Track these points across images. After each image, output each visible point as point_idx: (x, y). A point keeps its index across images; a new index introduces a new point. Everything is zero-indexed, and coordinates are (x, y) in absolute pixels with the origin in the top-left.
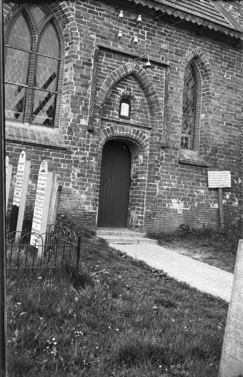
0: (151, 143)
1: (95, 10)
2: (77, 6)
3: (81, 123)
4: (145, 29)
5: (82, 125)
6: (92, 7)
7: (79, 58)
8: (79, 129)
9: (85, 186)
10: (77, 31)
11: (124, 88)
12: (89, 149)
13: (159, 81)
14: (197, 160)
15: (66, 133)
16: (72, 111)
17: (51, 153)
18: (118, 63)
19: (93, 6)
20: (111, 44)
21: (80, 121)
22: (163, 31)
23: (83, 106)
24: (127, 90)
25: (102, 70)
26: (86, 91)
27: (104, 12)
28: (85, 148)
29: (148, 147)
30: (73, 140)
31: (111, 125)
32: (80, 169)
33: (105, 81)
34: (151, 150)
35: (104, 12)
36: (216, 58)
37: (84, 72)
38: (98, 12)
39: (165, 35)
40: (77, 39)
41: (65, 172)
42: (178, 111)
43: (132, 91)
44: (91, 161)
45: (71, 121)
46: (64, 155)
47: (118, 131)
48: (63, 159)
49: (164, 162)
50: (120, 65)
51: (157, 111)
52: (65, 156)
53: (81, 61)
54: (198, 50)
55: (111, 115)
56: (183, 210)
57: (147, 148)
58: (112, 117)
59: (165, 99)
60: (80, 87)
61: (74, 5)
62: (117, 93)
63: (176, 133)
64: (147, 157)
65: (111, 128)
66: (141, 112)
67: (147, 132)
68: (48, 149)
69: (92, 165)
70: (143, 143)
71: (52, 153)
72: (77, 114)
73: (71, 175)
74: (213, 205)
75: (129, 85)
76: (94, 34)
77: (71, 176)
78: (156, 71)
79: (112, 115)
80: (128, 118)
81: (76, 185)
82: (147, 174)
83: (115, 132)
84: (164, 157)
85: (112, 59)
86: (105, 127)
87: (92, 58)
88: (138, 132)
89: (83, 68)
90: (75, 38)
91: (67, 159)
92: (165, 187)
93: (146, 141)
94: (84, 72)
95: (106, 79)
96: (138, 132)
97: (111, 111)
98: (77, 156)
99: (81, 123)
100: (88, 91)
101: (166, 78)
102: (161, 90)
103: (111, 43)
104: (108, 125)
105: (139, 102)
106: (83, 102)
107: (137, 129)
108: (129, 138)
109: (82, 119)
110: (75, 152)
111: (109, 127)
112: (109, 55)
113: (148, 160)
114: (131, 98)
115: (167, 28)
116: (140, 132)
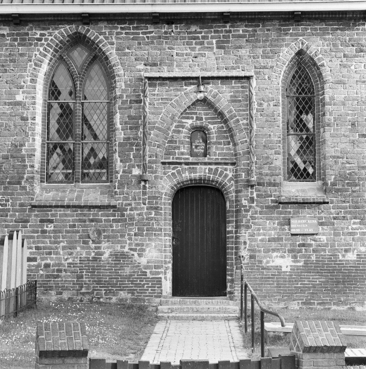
0: (236, 182)
1: (141, 35)
2: (118, 38)
3: (133, 173)
4: (212, 38)
5: (135, 176)
6: (136, 32)
7: (125, 96)
8: (132, 181)
11: (192, 118)
13: (240, 99)
14: (303, 195)
15: (116, 188)
16: (121, 161)
17: (100, 213)
19: (138, 31)
21: (131, 171)
22: (241, 31)
23: (134, 152)
24: (196, 120)
26: (137, 134)
27: (153, 34)
28: (141, 202)
29: (233, 188)
31: (178, 167)
32: (137, 227)
33: (161, 116)
35: (153, 34)
36: (334, 45)
37: (133, 112)
38: (145, 36)
39: (244, 36)
41: (119, 233)
43: (204, 120)
44: (150, 216)
45: (121, 173)
48: (114, 218)
52: (117, 215)
53: (127, 100)
54: (300, 42)
56: (291, 266)
57: (231, 189)
60: (128, 131)
61: (113, 37)
62: (183, 127)
64: (233, 200)
65: (179, 172)
66: (220, 143)
68: (96, 210)
69: (152, 220)
70: (226, 183)
71: (101, 214)
72: (128, 164)
73: (126, 235)
74: (344, 256)
75: (200, 113)
76: (141, 64)
77: (127, 237)
79: (178, 155)
81: (133, 247)
83: (183, 175)
86: (169, 172)
87: (141, 93)
88: (217, 169)
89: (131, 108)
91: (119, 218)
92: (260, 238)
94: (133, 112)
96: (217, 169)
97: (177, 151)
98: (132, 212)
99: (133, 173)
100: (139, 133)
102: (244, 111)
104: (173, 169)
105: (215, 131)
106: (134, 148)
107: (213, 167)
109: (135, 168)
110: (129, 207)
111: (174, 171)
114: (205, 129)
115: (246, 26)
116: (220, 170)
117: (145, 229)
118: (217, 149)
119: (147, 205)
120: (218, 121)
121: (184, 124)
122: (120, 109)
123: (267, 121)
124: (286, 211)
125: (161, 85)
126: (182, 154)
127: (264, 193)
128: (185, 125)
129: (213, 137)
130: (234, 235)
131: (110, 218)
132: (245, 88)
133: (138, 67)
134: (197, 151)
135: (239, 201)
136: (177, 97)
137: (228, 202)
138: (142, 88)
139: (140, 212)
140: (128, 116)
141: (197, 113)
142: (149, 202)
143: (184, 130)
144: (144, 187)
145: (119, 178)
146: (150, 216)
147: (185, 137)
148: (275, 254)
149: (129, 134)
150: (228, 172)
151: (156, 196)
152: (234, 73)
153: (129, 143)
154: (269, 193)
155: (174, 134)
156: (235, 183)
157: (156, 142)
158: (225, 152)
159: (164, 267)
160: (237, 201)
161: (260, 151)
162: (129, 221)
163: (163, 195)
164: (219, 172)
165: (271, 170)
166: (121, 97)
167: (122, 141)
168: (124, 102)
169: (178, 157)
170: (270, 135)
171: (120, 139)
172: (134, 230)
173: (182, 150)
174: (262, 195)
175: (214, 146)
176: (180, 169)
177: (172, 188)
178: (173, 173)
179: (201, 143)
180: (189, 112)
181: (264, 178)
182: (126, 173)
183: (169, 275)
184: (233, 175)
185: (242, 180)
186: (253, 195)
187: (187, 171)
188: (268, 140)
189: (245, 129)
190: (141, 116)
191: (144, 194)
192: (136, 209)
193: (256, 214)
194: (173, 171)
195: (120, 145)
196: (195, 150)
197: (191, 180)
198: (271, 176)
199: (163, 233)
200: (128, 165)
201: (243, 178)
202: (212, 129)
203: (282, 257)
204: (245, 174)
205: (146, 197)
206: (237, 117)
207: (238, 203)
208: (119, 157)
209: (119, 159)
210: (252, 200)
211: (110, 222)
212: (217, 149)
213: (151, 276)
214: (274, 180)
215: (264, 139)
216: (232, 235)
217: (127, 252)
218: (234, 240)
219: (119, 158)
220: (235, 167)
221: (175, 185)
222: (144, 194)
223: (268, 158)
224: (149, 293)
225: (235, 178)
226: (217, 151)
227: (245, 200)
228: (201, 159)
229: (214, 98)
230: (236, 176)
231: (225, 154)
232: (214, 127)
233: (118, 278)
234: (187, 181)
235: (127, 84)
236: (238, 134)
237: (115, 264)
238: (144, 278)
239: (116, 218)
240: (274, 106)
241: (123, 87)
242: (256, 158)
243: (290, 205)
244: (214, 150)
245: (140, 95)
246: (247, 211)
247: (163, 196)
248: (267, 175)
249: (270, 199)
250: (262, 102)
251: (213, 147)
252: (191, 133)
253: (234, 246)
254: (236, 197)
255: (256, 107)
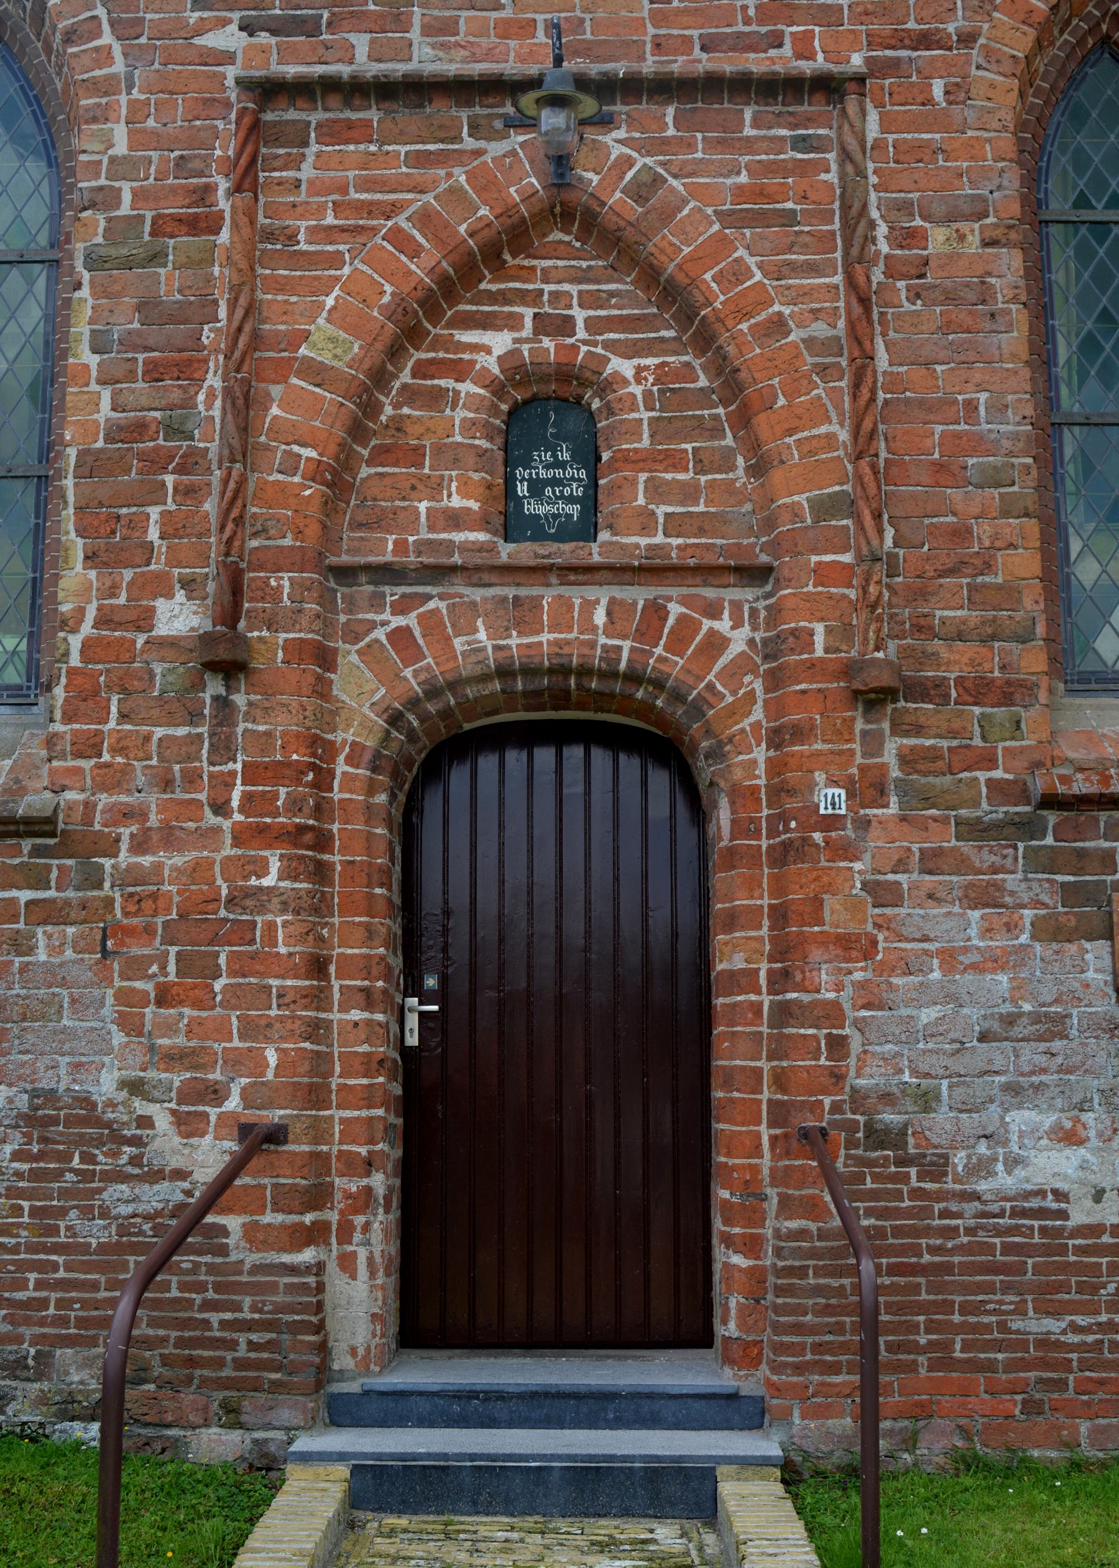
0: (774, 680)
3: (162, 629)
5: (171, 643)
7: (127, 197)
8: (152, 675)
9: (216, 1075)
10: (107, 38)
11: (513, 323)
12: (235, 803)
13: (789, 205)
15: (58, 715)
16: (90, 558)
18: (420, 160)
20: (362, 52)
23: (171, 506)
24: (537, 331)
25: (301, 237)
26: (189, 403)
28: (203, 796)
29: (758, 713)
30: (106, 757)
32: (173, 950)
33: (330, 302)
34: (776, 739)
40: (108, 86)
42: (983, 397)
43: (581, 333)
44: (253, 881)
45: (87, 628)
46: (48, 868)
47: (482, 635)
49: (893, 809)
50: (442, 172)
51: (790, 432)
52: (54, 874)
55: (425, 535)
58: (425, 546)
59: (851, 325)
60: (141, 385)
62: (460, 371)
63: (988, 567)
65: (430, 622)
66: (676, 462)
67: (736, 606)
69: (262, 909)
70: (710, 687)
72: (128, 574)
75: (555, 296)
76: (226, 22)
78: (749, 145)
80: (587, 529)
82: (766, 923)
83: (459, 643)
84: (895, 773)
85: (373, 148)
86: (373, 625)
89: (156, 257)
90: (94, 81)
93: (733, 673)
94: (168, 282)
95: (336, 292)
96: (656, 611)
98: (146, 860)
100: (201, 397)
101: (842, 176)
102: (812, 269)
103: (361, 43)
104: (400, 608)
105: (648, 394)
106: (169, 480)
107: (639, 595)
108: (585, 671)
109: (170, 596)
111: (410, 620)
112: (350, 125)
113: (765, 812)
114: (584, 384)
116: (675, 610)
117: (222, 960)
118: (656, 492)
119: (238, 817)
120: (662, 340)
121: (466, 356)
122: (93, 262)
123: (947, 327)
124: (1081, 854)
125: (332, 133)
126: (455, 520)
127: (945, 744)
128: (473, 362)
129: (636, 422)
130: (766, 1000)
131: (14, 893)
132: (813, 149)
133: (213, 40)
134: (542, 510)
135: (791, 792)
136: (429, 198)
137: (724, 803)
138: (224, 148)
139: (191, 856)
140: (139, 308)
141: (541, 292)
142: (247, 797)
143: (467, 387)
144: (223, 704)
145: (75, 660)
146: (253, 881)
147: (469, 426)
148: (1020, 1119)
149: (144, 401)
150: (723, 625)
151: (289, 764)
152: (756, 63)
153: (142, 456)
154: (977, 742)
155: (406, 410)
156: (767, 691)
157: (296, 448)
158: (701, 508)
159: (338, 1196)
160: (778, 791)
161: (913, 496)
162: (126, 914)
163: (341, 759)
164: (671, 621)
165: (983, 606)
166: (106, 199)
167: (100, 444)
168: (119, 230)
169: (430, 542)
170: (971, 406)
171: (89, 429)
172: (154, 969)
173: (456, 502)
174: (933, 755)
175: (643, 477)
176: (442, 605)
177: (395, 719)
178: (398, 629)
179: (562, 465)
180: (494, 287)
181: (945, 654)
182: (120, 625)
183: (376, 1238)
184: (751, 642)
185: (812, 665)
186: (879, 752)
187: (480, 623)
188: (958, 435)
189: (823, 370)
190: (215, 302)
191: (223, 749)
192: (169, 838)
193: (900, 866)
194: (398, 621)
195: (91, 466)
196: (531, 507)
197: (504, 672)
198: (987, 640)
199: (336, 984)
200: (131, 584)
201: (819, 652)
202: (625, 382)
203: (1070, 1138)
204: (829, 631)
205: (231, 766)
206: (776, 308)
207: (791, 804)
208: (80, 533)
209: (78, 546)
210: (868, 789)
211: (15, 918)
212: (656, 492)
213: (253, 1258)
214: (1003, 668)
215: (939, 428)
216: (753, 997)
217: (111, 1104)
218: (765, 1029)
219: (80, 541)
220: (767, 596)
221: (413, 703)
222: (223, 749)
223: (961, 534)
224: (241, 1364)
225: (766, 658)
226: (646, 517)
227: (833, 782)
228: (566, 552)
229: (640, 199)
230: (771, 649)
231: (701, 525)
232: (639, 370)
233: (55, 1267)
234: (485, 678)
235: (144, 131)
236: (782, 401)
237: (34, 1175)
238: (212, 1269)
239: (51, 893)
240: (986, 244)
241: (121, 148)
242: (889, 533)
243: (1103, 816)
244: (641, 501)
245: (210, 189)
246: (846, 851)
247: (341, 767)
248: (960, 637)
249: (982, 776)
250: (918, 222)
251: (634, 482)
252: (504, 407)
253: (764, 1064)
254: (775, 767)
255: (884, 247)
